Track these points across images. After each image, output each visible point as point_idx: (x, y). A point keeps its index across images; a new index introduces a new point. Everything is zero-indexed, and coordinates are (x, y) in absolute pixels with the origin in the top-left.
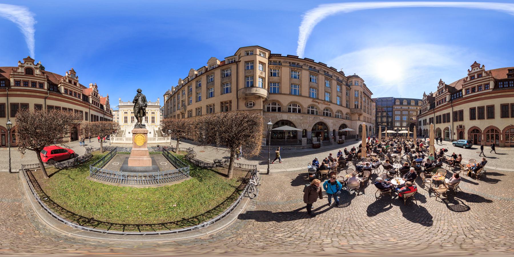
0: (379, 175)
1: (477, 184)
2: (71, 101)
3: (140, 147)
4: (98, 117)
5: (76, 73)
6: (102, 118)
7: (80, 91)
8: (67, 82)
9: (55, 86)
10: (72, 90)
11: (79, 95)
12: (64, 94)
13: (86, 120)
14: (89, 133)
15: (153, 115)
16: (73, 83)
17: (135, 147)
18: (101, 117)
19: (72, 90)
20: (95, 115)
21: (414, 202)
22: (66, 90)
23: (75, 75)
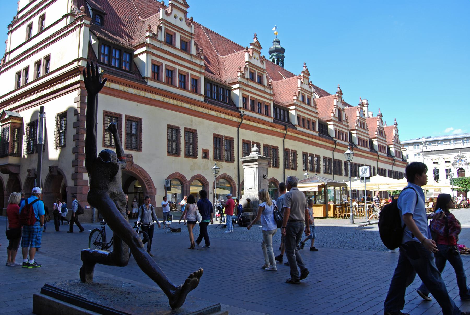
0: (405, 165)
1: (366, 124)
2: (255, 124)
3: (437, 192)
4: (385, 170)
5: (187, 6)
6: (330, 159)
7: (269, 97)
8: (161, 42)
9: (116, 49)
10: (161, 61)
11: (196, 82)
12: (151, 79)
13: (324, 173)
14: (123, 197)
15: (436, 165)
16: (178, 44)
17: (435, 192)
18: (325, 158)
19: (161, 61)
20: (382, 168)
21: (20, 213)
22: (156, 68)
23: (186, 13)
